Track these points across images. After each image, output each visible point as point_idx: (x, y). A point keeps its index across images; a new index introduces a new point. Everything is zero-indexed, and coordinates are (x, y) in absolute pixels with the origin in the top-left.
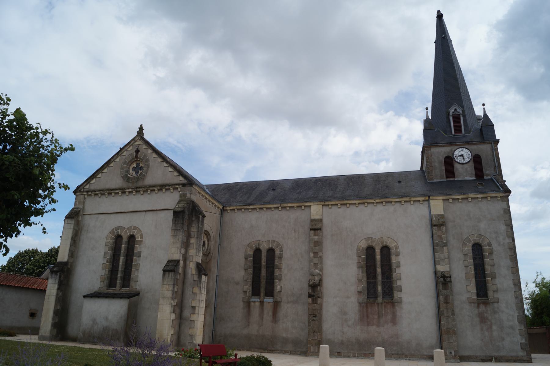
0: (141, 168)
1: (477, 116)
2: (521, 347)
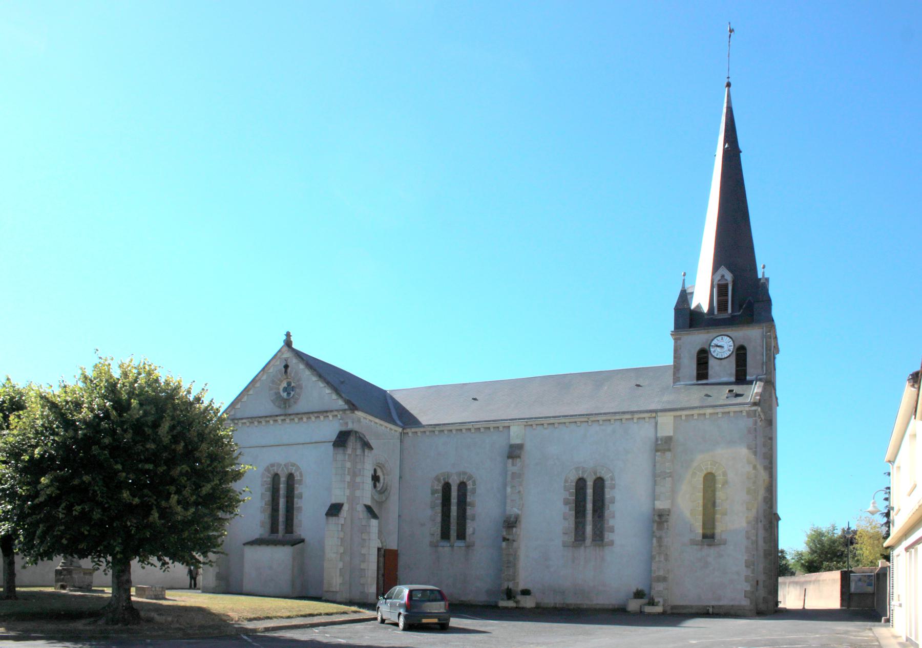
0: (293, 389)
1: (130, 563)
2: (745, 594)
